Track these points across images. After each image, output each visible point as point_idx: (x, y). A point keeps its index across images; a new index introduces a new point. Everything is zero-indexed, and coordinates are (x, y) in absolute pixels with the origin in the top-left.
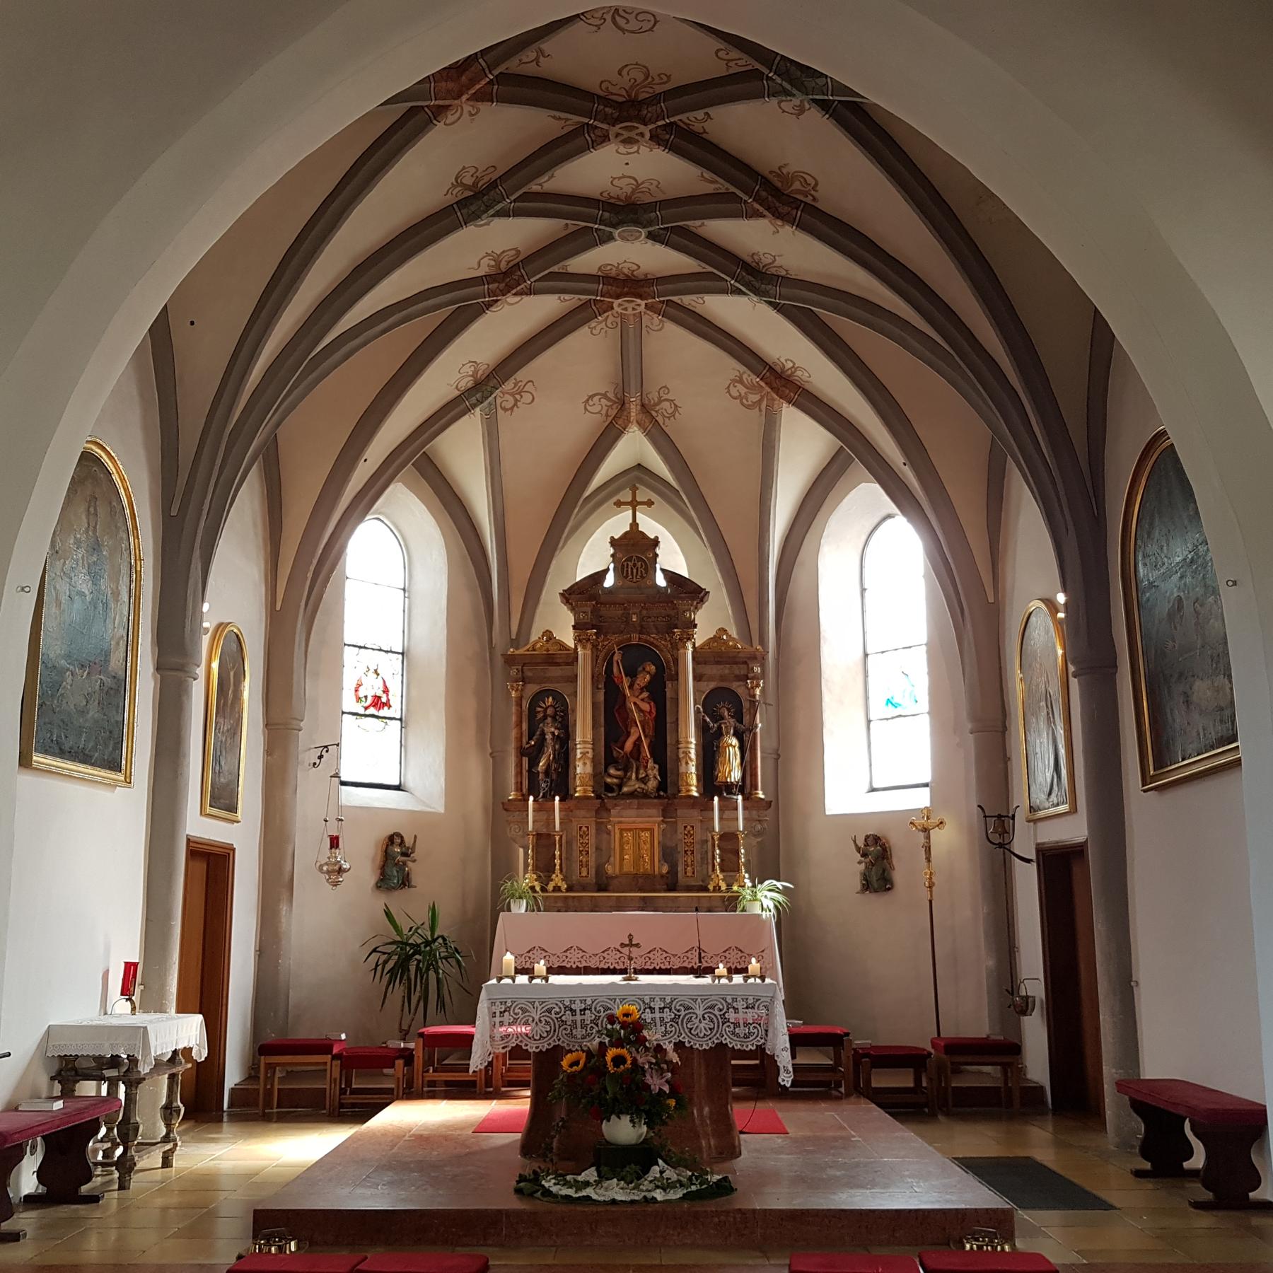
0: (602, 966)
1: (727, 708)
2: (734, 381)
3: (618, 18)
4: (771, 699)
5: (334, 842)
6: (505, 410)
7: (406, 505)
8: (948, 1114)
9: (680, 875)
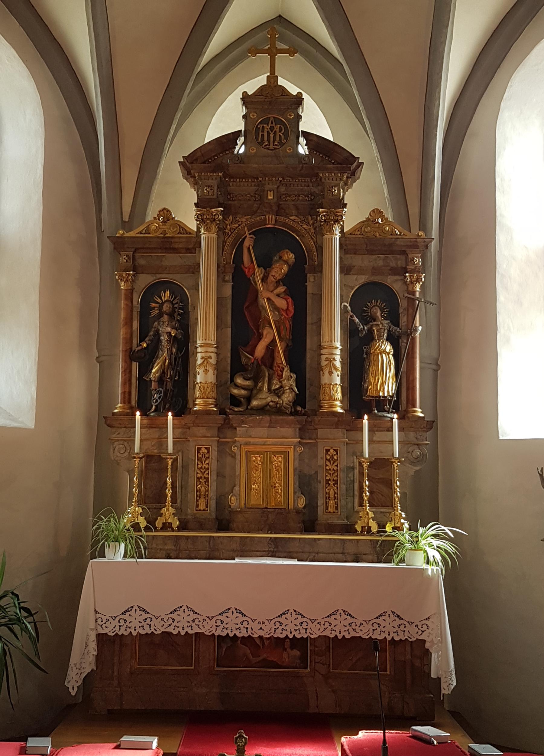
1: (382, 308)
4: (431, 297)
9: (321, 510)
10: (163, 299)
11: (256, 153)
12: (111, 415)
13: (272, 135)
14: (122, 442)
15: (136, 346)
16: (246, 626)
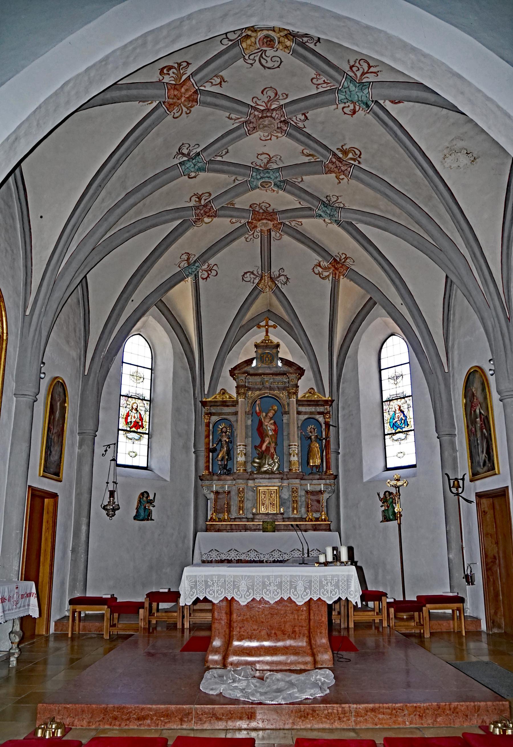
0: (247, 559)
2: (316, 265)
3: (262, 60)
5: (112, 494)
6: (203, 279)
7: (152, 322)
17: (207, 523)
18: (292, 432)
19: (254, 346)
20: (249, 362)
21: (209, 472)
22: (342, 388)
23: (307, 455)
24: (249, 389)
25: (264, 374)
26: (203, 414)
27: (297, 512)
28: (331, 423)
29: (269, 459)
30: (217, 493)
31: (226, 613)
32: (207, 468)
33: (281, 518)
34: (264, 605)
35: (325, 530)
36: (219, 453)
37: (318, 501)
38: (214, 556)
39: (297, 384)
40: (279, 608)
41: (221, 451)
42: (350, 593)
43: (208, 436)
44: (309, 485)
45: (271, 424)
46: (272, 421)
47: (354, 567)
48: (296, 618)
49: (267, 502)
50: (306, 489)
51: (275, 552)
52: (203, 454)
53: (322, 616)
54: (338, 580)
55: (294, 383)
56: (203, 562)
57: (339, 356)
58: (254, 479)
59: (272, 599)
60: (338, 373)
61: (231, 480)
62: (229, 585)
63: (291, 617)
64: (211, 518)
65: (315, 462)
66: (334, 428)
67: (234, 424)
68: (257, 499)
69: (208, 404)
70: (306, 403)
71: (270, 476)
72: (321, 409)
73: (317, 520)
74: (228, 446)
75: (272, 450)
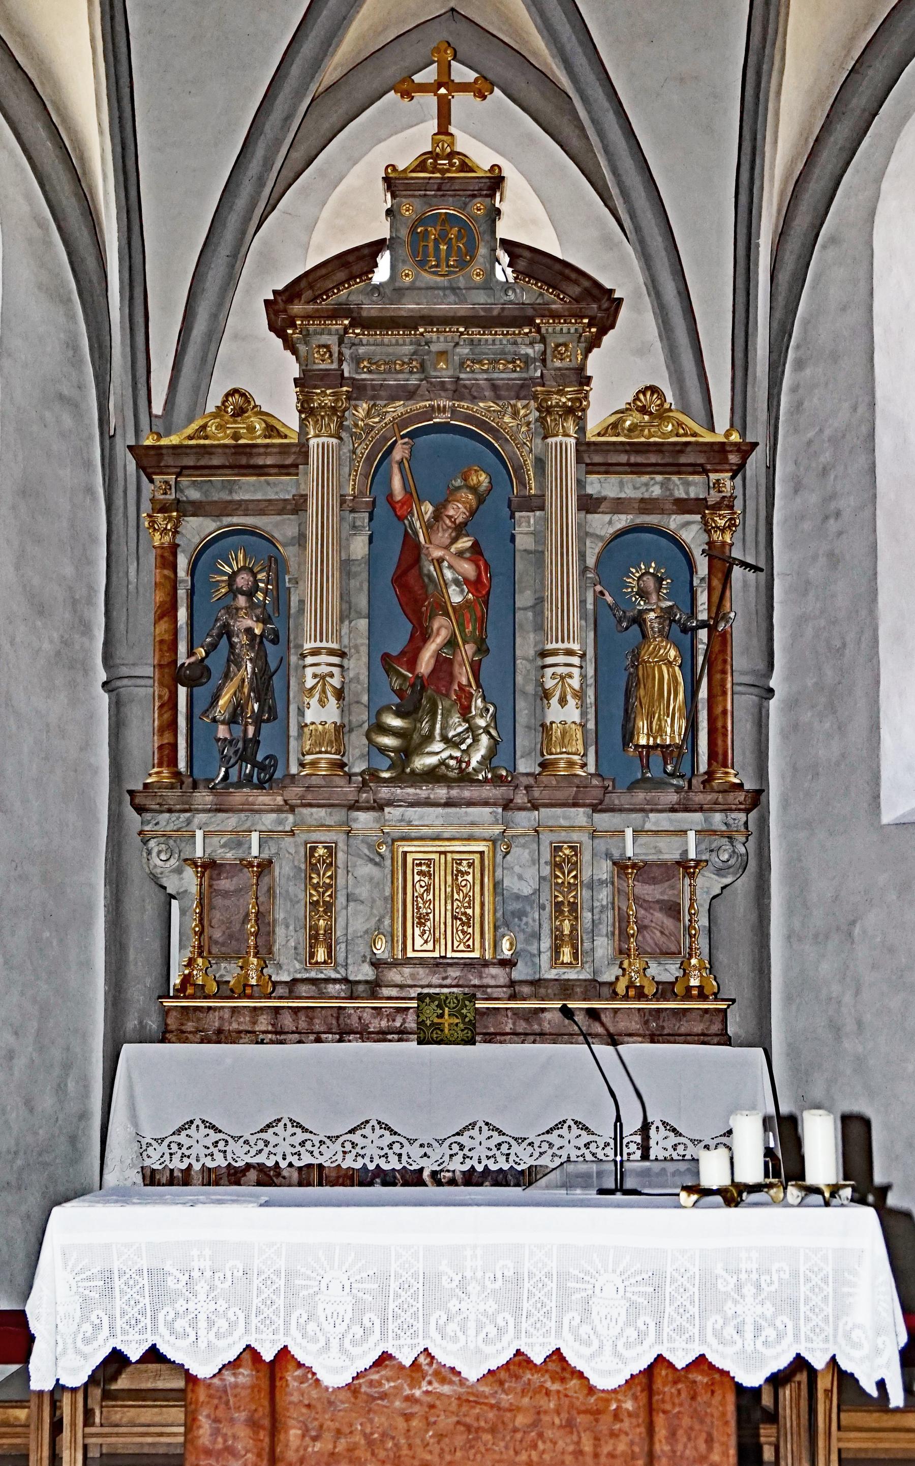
8: (109, 990)
10: (234, 564)
11: (413, 282)
12: (140, 787)
13: (443, 247)
14: (162, 839)
15: (185, 655)
16: (398, 1151)
17: (168, 1003)
18: (552, 593)
19: (380, 185)
20: (361, 259)
21: (177, 774)
22: (794, 389)
23: (621, 694)
24: (359, 390)
25: (429, 320)
26: (146, 506)
27: (575, 955)
28: (736, 553)
29: (446, 716)
30: (209, 868)
31: (253, 1424)
32: (168, 755)
33: (502, 981)
34: (437, 1387)
35: (703, 1039)
36: (220, 689)
37: (673, 910)
38: (200, 1152)
39: (582, 368)
40: (506, 1399)
41: (227, 676)
42: (848, 1336)
43: (168, 611)
44: (629, 833)
45: (460, 554)
46: (465, 543)
47: (871, 1211)
48: (588, 1447)
49: (441, 911)
50: (616, 855)
51: (475, 1132)
52: (144, 697)
53: (709, 1440)
54: (795, 1274)
55: (566, 363)
56: (151, 1178)
57: (781, 237)
58: (379, 806)
59: (473, 1357)
60: (778, 315)
61: (278, 810)
62: (267, 1293)
63: (561, 1444)
64: (187, 980)
65: (661, 730)
66: (751, 575)
67: (289, 553)
68: (392, 898)
69: (169, 460)
70: (623, 458)
71: (454, 792)
72: (692, 487)
73: (665, 990)
74: (261, 659)
75: (463, 675)
